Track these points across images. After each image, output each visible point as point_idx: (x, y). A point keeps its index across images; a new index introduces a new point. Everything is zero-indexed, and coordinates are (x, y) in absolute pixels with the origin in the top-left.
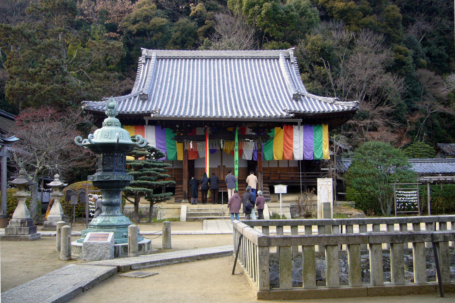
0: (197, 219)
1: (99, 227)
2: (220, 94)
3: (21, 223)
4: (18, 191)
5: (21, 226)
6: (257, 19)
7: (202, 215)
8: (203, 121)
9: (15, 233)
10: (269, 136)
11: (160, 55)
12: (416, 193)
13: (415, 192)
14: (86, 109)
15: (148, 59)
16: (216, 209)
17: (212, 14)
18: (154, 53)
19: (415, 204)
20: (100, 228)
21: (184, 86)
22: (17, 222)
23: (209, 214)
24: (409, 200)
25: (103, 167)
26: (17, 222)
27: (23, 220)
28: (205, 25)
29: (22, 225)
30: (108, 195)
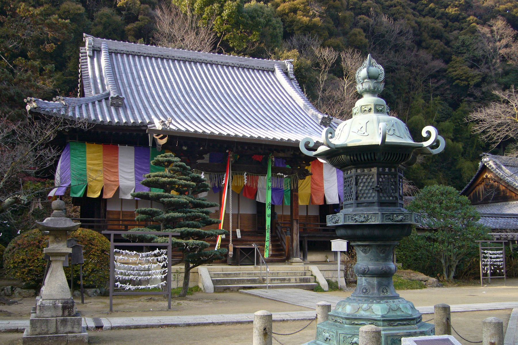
0: (228, 288)
1: (386, 323)
2: (232, 108)
3: (64, 308)
4: (53, 242)
5: (63, 315)
6: (216, 22)
7: (233, 282)
8: (234, 142)
9: (53, 330)
10: (307, 171)
11: (114, 48)
12: (502, 254)
13: (501, 252)
14: (34, 111)
15: (96, 51)
16: (250, 274)
17: (147, 8)
18: (104, 44)
19: (501, 267)
20: (390, 325)
21: (251, 82)
22: (55, 307)
23: (242, 281)
24: (495, 262)
25: (379, 197)
26: (55, 307)
27: (67, 303)
28: (139, 21)
29: (66, 313)
30: (381, 255)
